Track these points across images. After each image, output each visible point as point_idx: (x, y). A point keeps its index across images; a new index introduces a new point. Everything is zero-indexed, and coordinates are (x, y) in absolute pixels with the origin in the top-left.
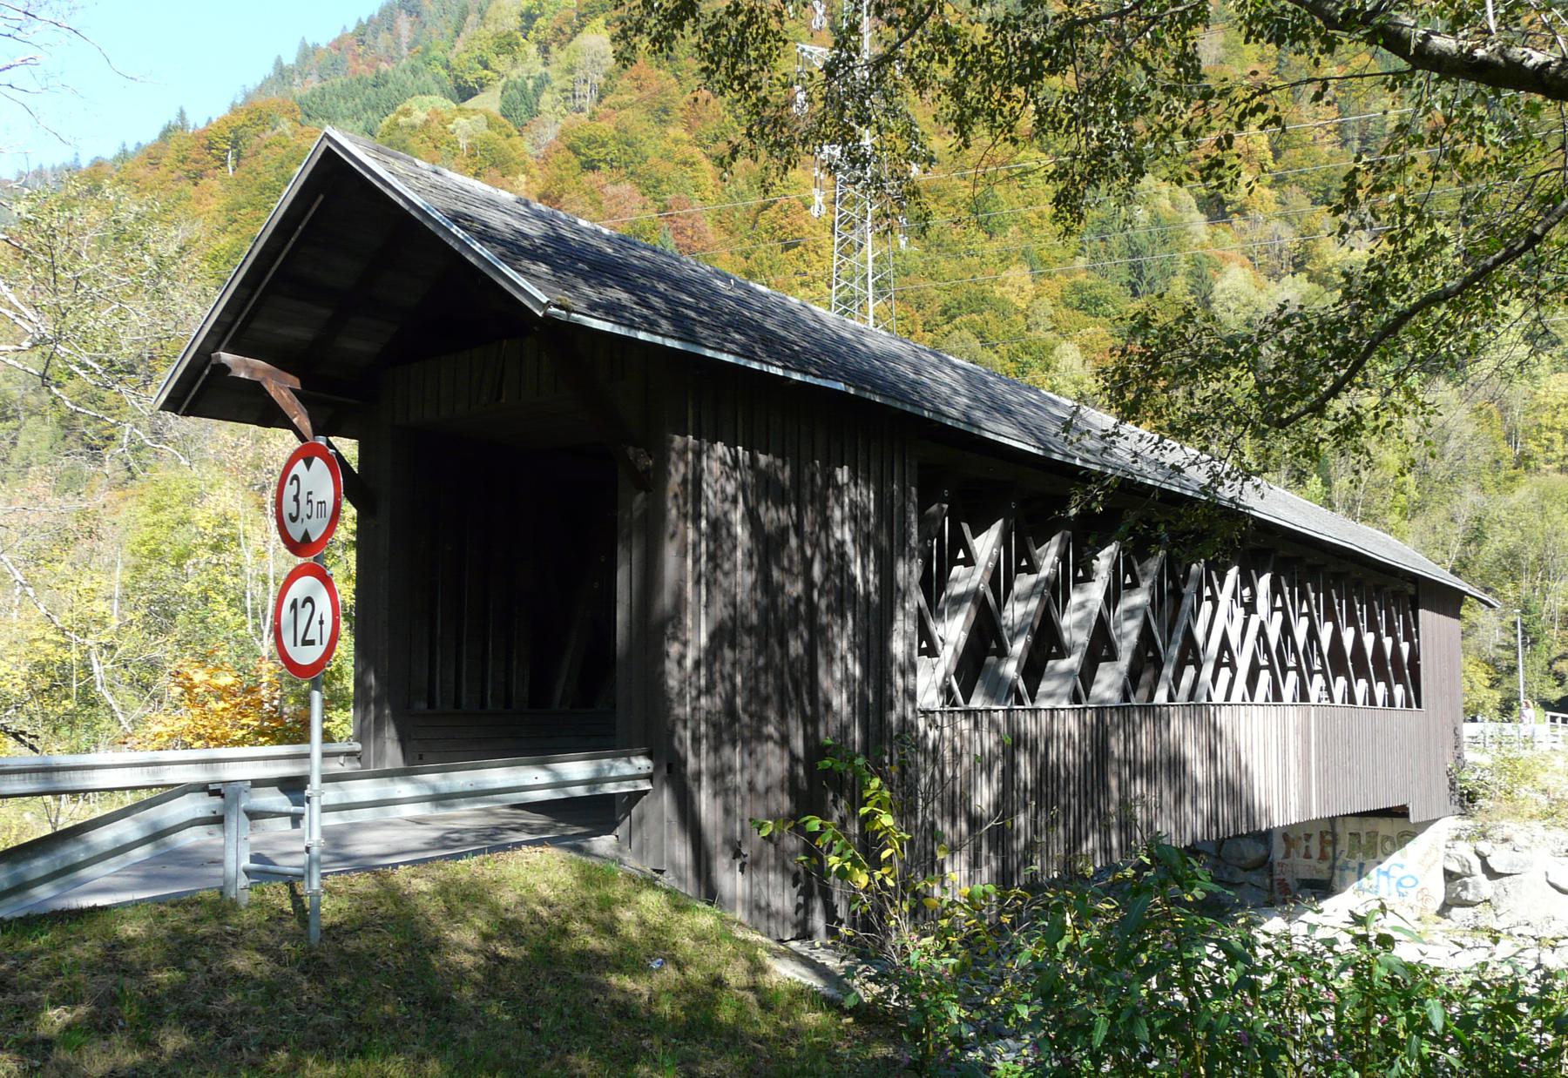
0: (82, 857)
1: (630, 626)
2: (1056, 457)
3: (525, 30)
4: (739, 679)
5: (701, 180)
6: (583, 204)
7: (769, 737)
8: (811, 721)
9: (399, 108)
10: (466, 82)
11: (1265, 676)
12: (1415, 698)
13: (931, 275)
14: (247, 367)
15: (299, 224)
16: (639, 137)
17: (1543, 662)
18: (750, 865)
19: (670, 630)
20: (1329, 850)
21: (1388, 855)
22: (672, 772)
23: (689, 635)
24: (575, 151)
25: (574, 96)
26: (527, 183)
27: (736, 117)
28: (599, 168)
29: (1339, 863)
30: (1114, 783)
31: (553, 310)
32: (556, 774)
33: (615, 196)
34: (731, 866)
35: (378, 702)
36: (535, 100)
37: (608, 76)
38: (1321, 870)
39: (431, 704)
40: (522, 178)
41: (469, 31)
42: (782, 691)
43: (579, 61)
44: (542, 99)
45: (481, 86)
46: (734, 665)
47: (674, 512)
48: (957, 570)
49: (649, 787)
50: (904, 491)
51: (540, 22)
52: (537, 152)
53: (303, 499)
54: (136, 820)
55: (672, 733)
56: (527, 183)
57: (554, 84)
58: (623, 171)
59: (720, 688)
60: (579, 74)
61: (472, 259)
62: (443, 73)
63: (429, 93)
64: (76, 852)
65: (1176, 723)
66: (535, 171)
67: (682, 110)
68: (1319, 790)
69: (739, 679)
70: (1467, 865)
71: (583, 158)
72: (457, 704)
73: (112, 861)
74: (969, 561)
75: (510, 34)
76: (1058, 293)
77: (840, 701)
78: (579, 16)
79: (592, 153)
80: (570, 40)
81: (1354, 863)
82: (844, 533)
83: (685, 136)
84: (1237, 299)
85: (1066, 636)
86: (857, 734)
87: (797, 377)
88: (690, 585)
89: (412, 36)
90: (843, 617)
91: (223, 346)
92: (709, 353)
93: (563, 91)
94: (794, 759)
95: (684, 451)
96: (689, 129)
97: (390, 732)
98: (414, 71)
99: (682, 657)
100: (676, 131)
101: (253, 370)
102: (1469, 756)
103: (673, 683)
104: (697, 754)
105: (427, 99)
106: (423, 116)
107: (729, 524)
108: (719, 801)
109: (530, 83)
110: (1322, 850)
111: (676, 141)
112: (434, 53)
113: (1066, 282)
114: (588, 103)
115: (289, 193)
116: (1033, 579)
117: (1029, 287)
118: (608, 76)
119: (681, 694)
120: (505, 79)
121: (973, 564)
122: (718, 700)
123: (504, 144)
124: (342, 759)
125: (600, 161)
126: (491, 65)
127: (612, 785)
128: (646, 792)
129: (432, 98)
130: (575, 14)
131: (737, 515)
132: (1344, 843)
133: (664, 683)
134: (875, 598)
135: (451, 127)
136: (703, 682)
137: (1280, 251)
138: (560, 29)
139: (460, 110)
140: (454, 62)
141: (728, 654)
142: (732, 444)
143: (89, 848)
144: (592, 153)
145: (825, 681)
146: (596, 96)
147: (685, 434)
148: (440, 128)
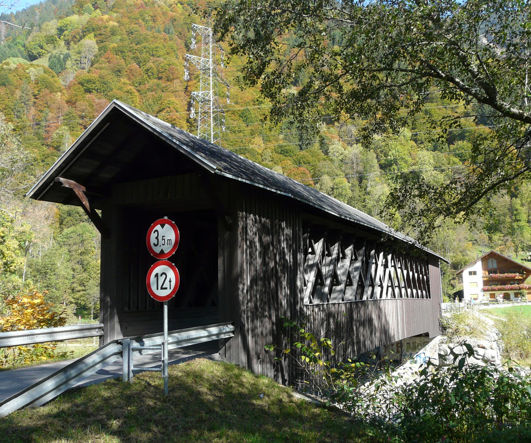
0: (85, 368)
1: (224, 278)
2: (343, 217)
3: (59, 35)
4: (258, 296)
5: (134, 99)
6: (86, 106)
7: (266, 316)
8: (277, 310)
9: (4, 62)
10: (33, 53)
11: (390, 289)
12: (429, 296)
13: (226, 139)
14: (68, 183)
15: (98, 132)
16: (109, 81)
17: (448, 281)
18: (262, 362)
19: (240, 280)
20: (400, 349)
21: (420, 350)
22: (240, 330)
23: (245, 281)
24: (82, 84)
25: (81, 63)
26: (61, 96)
27: (149, 76)
28: (92, 92)
29: (403, 354)
30: (355, 328)
31: (217, 171)
32: (209, 332)
33: (99, 104)
34: (257, 362)
35: (112, 307)
36: (64, 63)
37: (96, 56)
38: (397, 357)
39: (129, 309)
40: (59, 94)
41: (34, 34)
42: (269, 301)
43: (83, 49)
44: (67, 63)
45: (40, 56)
46: (257, 291)
47: (240, 238)
48: (310, 256)
49: (233, 335)
50: (299, 229)
51: (66, 32)
52: (66, 84)
53: (160, 238)
54: (98, 354)
55: (241, 315)
56: (61, 96)
57: (72, 57)
58: (102, 94)
59: (253, 300)
60: (83, 54)
61: (182, 151)
62: (23, 49)
63: (17, 56)
64: (81, 366)
65: (370, 307)
66: (65, 91)
67: (126, 71)
68: (406, 328)
69: (258, 296)
70: (445, 351)
71: (85, 88)
72: (138, 308)
73: (91, 370)
74: (313, 253)
75: (52, 36)
76: (273, 148)
77: (284, 302)
78: (83, 32)
79: (89, 86)
80: (79, 41)
81: (408, 353)
82: (284, 245)
83: (128, 82)
84: (338, 152)
85: (339, 278)
86: (289, 314)
87: (279, 192)
88: (245, 264)
89: (7, 32)
90: (284, 274)
91: (60, 175)
92: (257, 185)
93: (76, 60)
94: (273, 323)
95: (242, 218)
96: (129, 79)
97: (116, 319)
98: (9, 47)
99: (243, 289)
100: (124, 80)
101: (70, 184)
102: (443, 314)
103: (241, 298)
104: (248, 323)
105: (15, 59)
106: (15, 66)
107: (254, 243)
108: (254, 339)
109: (62, 56)
110: (397, 349)
111: (124, 84)
112: (18, 41)
113: (276, 144)
114: (87, 66)
115: (96, 122)
116: (330, 258)
117: (263, 145)
118: (96, 56)
119: (243, 302)
120: (50, 54)
121: (315, 254)
122: (253, 304)
123: (52, 80)
124: (97, 330)
125: (92, 89)
126: (44, 47)
127: (223, 335)
128: (232, 337)
129: (18, 59)
130: (81, 31)
131: (257, 239)
132: (405, 347)
133: (239, 298)
134: (292, 267)
135: (27, 71)
136: (249, 298)
137: (351, 135)
138: (75, 36)
139: (31, 65)
140: (27, 45)
141: (255, 287)
142: (255, 215)
143: (86, 365)
144: (89, 86)
145: (280, 296)
146: (90, 64)
147: (242, 212)
148: (23, 71)
